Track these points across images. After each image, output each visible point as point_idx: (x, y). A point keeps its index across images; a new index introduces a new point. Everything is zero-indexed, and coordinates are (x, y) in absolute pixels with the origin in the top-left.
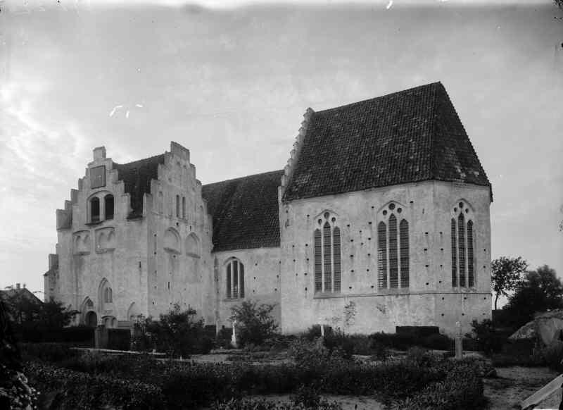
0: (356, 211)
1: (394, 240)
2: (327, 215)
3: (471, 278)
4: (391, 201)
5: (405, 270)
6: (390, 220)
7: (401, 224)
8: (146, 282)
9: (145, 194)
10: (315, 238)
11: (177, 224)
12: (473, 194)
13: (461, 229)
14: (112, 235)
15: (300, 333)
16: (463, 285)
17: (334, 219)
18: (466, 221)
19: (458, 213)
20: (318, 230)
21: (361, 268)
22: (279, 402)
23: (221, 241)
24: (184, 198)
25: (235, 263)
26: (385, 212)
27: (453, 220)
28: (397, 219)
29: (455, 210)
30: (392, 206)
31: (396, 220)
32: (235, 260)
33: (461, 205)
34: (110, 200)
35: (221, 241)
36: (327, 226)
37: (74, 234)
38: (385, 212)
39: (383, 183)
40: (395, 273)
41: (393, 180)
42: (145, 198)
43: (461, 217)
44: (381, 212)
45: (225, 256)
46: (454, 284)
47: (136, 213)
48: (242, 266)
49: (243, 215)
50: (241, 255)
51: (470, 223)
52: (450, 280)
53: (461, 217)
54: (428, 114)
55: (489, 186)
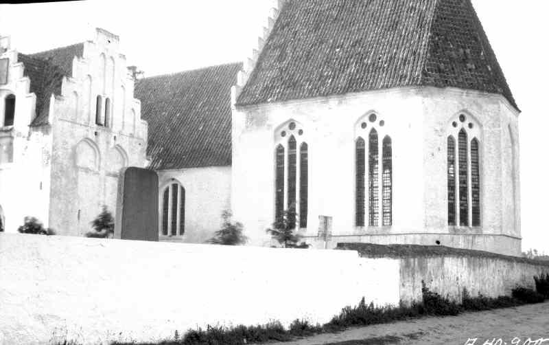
3: (476, 212)
4: (373, 111)
9: (53, 95)
11: (96, 134)
12: (488, 109)
13: (463, 149)
14: (176, 150)
15: (395, 322)
19: (368, 129)
22: (114, 334)
24: (107, 100)
25: (175, 187)
26: (364, 125)
27: (451, 139)
29: (455, 124)
30: (373, 118)
32: (174, 182)
33: (462, 118)
38: (364, 125)
39: (354, 86)
42: (52, 98)
43: (463, 134)
44: (360, 124)
46: (451, 220)
47: (39, 120)
48: (183, 190)
52: (445, 214)
53: (463, 134)
54: (342, 20)
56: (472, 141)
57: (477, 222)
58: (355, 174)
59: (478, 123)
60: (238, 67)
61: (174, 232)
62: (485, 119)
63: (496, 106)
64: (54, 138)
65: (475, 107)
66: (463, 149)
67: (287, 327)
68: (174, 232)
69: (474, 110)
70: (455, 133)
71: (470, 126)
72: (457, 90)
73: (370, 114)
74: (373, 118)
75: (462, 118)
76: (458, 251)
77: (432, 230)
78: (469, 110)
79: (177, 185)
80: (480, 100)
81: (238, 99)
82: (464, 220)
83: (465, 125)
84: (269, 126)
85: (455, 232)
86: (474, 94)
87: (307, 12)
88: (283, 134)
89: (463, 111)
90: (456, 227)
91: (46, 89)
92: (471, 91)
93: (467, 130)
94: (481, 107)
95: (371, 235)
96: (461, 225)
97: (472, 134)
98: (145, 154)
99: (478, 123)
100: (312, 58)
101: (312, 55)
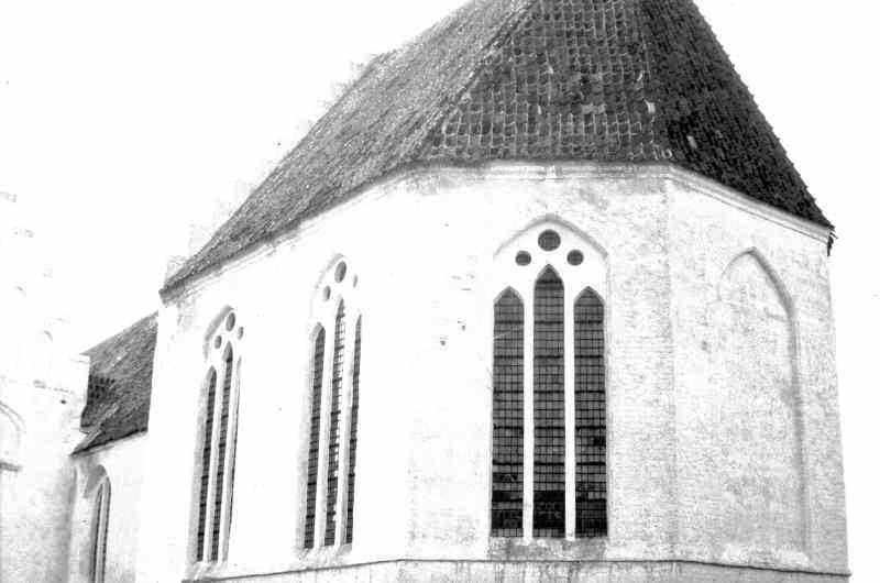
13: (549, 323)
33: (549, 241)
46: (504, 518)
56: (578, 305)
57: (594, 522)
59: (596, 247)
62: (611, 232)
63: (658, 197)
65: (586, 207)
66: (549, 323)
69: (579, 214)
70: (524, 283)
72: (528, 170)
73: (337, 264)
77: (428, 550)
78: (566, 217)
80: (600, 188)
82: (548, 521)
83: (557, 259)
84: (198, 327)
85: (510, 554)
86: (579, 176)
90: (517, 542)
91: (655, 431)
92: (572, 167)
94: (602, 206)
95: (317, 570)
96: (536, 536)
98: (77, 422)
99: (596, 247)
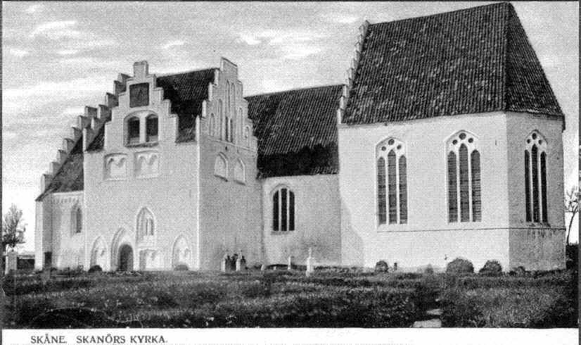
0: (426, 142)
1: (463, 171)
2: (391, 142)
4: (462, 131)
5: (451, 170)
6: (389, 156)
7: (472, 155)
8: (164, 215)
10: (379, 166)
16: (537, 221)
17: (399, 147)
18: (540, 152)
19: (458, 145)
20: (381, 158)
21: (428, 189)
23: (268, 165)
25: (284, 191)
26: (529, 141)
27: (526, 153)
28: (468, 148)
30: (462, 136)
31: (395, 155)
33: (534, 136)
34: (152, 123)
35: (268, 165)
36: (392, 155)
37: (108, 156)
40: (463, 203)
41: (464, 108)
45: (273, 184)
46: (528, 219)
48: (292, 194)
49: (294, 138)
50: (291, 182)
51: (475, 153)
53: (535, 149)
55: (563, 118)
58: (305, 176)
60: (340, 88)
61: (284, 228)
64: (475, 144)
67: (478, 267)
68: (284, 228)
71: (540, 142)
74: (462, 136)
75: (534, 136)
76: (49, 214)
79: (286, 190)
81: (344, 117)
87: (128, 45)
88: (384, 149)
89: (536, 130)
93: (538, 145)
97: (542, 148)
100: (388, 84)
101: (387, 81)
